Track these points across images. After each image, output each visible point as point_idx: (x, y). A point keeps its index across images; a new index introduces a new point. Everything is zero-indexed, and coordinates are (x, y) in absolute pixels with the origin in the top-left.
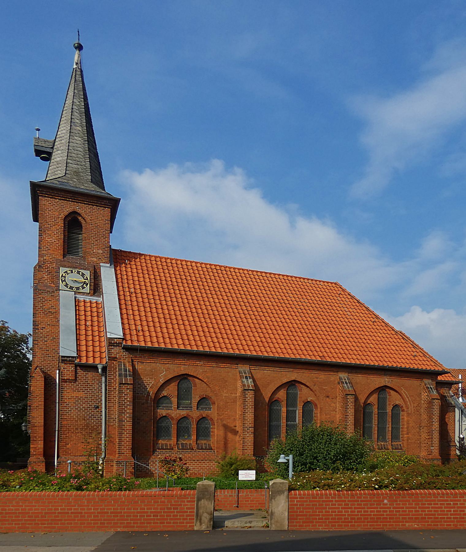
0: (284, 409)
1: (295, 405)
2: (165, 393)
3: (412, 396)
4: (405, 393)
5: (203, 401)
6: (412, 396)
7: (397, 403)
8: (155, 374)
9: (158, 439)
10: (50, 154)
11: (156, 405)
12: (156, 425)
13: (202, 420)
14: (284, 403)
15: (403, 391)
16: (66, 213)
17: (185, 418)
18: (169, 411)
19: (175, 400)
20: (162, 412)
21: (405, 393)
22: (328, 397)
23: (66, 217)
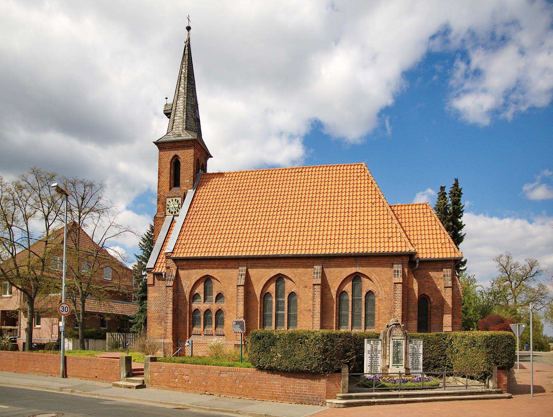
0: (274, 300)
1: (283, 296)
2: (196, 291)
3: (383, 281)
4: (376, 278)
5: (220, 296)
6: (383, 281)
7: (370, 289)
8: (190, 278)
9: (193, 327)
10: (66, 377)
11: (191, 300)
12: (191, 316)
13: (219, 312)
14: (274, 295)
15: (373, 277)
16: (171, 158)
17: (521, 350)
18: (199, 305)
19: (202, 296)
20: (195, 306)
21: (376, 278)
22: (306, 287)
23: (172, 160)
